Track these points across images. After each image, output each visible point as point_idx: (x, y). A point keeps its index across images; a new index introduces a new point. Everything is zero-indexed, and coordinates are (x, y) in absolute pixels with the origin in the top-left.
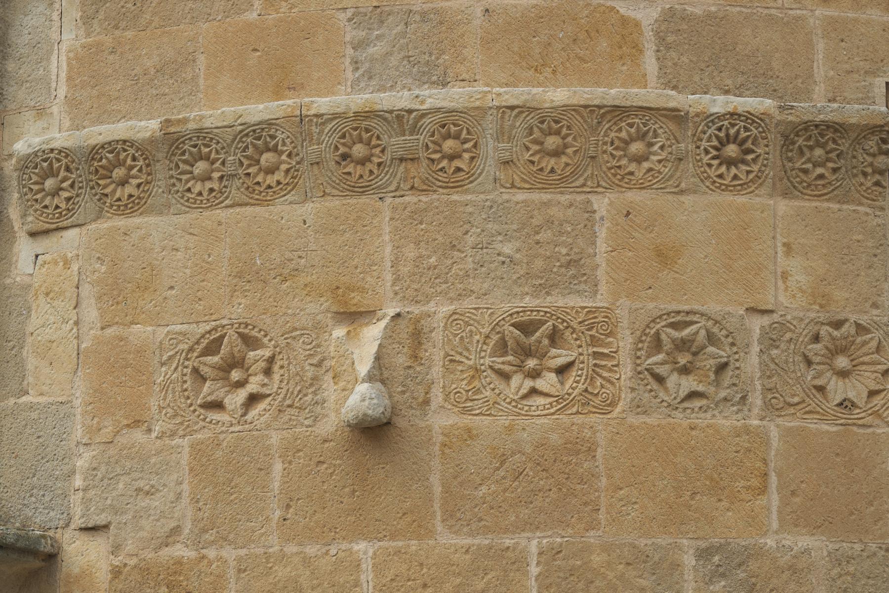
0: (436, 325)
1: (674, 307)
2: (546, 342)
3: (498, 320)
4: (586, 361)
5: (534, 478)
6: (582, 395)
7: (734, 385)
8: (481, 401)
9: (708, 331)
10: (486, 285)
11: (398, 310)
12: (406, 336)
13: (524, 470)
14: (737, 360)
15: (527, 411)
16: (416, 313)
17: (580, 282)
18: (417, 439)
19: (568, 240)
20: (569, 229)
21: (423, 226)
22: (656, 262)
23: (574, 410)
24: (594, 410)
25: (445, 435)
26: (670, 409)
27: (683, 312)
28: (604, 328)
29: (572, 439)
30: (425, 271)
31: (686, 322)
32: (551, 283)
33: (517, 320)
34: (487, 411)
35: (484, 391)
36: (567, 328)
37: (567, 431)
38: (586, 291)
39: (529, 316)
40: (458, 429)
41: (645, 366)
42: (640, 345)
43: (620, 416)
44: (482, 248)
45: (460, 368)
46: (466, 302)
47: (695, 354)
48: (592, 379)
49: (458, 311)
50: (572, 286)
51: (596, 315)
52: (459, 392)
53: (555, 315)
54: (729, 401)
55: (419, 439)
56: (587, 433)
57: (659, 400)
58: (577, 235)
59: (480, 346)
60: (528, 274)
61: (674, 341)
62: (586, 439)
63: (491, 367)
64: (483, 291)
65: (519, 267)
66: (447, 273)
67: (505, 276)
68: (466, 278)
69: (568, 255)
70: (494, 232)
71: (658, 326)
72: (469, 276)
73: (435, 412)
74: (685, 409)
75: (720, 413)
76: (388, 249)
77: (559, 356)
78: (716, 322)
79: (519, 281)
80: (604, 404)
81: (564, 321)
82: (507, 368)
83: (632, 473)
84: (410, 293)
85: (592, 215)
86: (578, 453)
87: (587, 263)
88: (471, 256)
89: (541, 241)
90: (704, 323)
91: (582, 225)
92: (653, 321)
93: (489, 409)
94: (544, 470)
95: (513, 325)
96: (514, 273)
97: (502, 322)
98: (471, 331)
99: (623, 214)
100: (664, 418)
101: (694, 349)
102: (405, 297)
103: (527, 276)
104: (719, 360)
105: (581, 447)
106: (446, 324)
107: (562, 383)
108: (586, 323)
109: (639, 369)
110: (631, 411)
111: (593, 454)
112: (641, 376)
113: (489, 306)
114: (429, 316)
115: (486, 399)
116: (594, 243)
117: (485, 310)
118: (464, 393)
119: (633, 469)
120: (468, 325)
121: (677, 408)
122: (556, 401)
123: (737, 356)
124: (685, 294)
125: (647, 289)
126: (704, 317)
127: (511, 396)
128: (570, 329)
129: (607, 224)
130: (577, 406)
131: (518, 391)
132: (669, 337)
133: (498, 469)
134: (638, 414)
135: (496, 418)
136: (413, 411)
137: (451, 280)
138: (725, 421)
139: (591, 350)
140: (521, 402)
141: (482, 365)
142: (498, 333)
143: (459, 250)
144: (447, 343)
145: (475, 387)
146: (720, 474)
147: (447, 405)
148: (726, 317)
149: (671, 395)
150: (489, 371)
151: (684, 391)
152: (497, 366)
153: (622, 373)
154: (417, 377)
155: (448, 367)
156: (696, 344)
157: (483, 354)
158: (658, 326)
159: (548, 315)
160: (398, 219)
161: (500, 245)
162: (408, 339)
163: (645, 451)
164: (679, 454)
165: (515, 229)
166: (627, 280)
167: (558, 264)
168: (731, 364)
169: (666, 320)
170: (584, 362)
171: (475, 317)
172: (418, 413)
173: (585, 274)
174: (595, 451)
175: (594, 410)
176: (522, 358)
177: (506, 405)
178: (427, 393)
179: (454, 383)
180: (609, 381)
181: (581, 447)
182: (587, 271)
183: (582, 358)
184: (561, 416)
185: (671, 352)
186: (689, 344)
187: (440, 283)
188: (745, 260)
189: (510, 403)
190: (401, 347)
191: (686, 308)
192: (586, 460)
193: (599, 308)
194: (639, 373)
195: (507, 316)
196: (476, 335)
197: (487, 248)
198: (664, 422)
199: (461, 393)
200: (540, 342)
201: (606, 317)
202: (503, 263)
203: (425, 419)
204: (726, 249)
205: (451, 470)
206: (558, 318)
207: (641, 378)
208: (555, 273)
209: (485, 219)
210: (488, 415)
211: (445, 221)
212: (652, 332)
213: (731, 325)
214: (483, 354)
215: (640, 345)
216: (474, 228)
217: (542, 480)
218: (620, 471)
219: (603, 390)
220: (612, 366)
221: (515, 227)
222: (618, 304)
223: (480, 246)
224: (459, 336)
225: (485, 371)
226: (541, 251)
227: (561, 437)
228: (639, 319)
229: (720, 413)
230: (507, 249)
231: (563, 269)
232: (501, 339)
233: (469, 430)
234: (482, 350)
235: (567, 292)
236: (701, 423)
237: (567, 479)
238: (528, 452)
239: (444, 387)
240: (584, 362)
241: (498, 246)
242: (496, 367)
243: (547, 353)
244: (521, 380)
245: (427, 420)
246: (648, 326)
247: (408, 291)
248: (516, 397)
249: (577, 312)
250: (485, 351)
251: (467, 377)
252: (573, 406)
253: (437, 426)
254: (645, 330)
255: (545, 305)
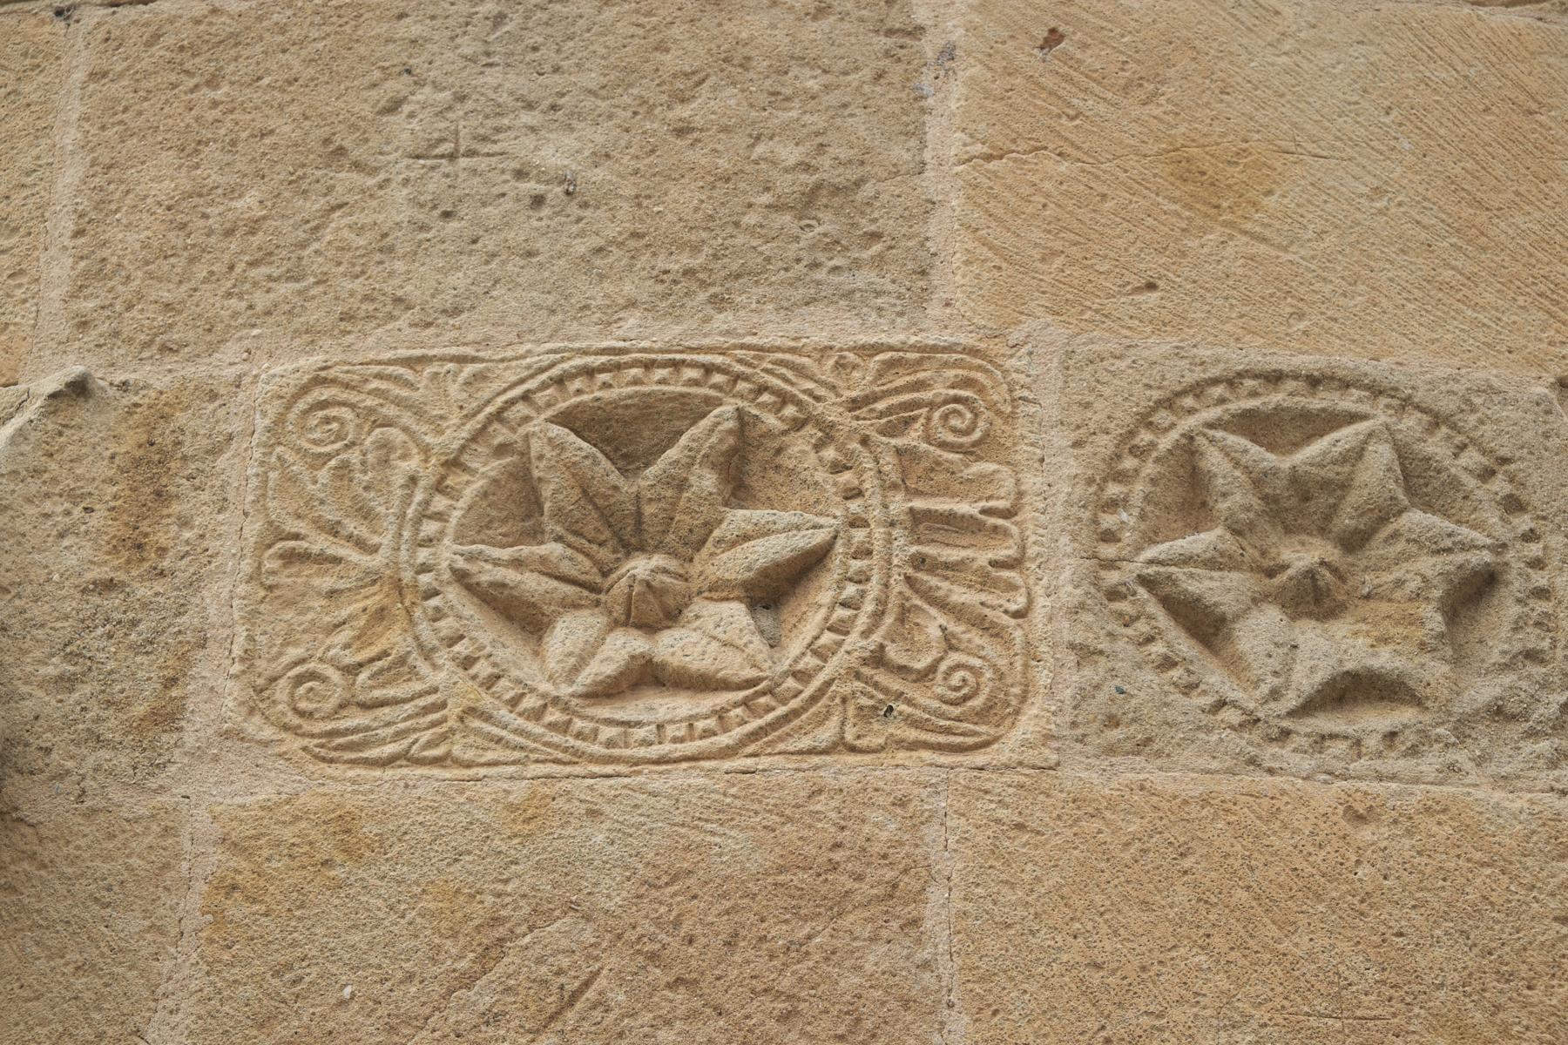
0: (236, 426)
1: (1256, 355)
2: (706, 481)
3: (500, 401)
4: (877, 546)
5: (633, 1015)
6: (858, 676)
7: (1532, 655)
8: (409, 708)
9: (1402, 452)
10: (458, 280)
11: (75, 370)
12: (103, 469)
13: (587, 984)
14: (1537, 564)
15: (610, 743)
16: (158, 386)
17: (857, 264)
18: (105, 868)
19: (807, 118)
20: (811, 84)
21: (219, 94)
22: (1174, 200)
23: (826, 734)
24: (913, 734)
25: (235, 847)
26: (1256, 735)
27: (1296, 377)
28: (955, 422)
29: (810, 850)
30: (213, 240)
31: (1306, 416)
32: (735, 267)
33: (585, 397)
34: (430, 744)
35: (424, 668)
36: (798, 425)
37: (790, 820)
38: (878, 294)
39: (636, 382)
40: (297, 819)
41: (1137, 566)
42: (1113, 489)
43: (1030, 756)
44: (452, 157)
45: (327, 582)
46: (370, 340)
47: (1353, 542)
48: (904, 615)
49: (332, 373)
50: (820, 275)
51: (921, 375)
52: (313, 676)
53: (747, 379)
54: (1513, 717)
55: (118, 866)
56: (879, 826)
57: (1207, 701)
58: (845, 106)
59: (419, 496)
60: (636, 235)
61: (1258, 480)
62: (876, 848)
63: (461, 577)
64: (447, 299)
65: (601, 213)
66: (303, 245)
67: (541, 244)
68: (378, 257)
69: (807, 167)
70: (504, 98)
71: (1191, 422)
72: (390, 249)
73: (197, 754)
74: (1323, 739)
75: (1479, 761)
76: (70, 176)
77: (764, 532)
78: (1437, 420)
79: (598, 262)
80: (956, 711)
81: (784, 399)
82: (532, 584)
83: (1086, 991)
84: (146, 316)
85: (908, 41)
86: (838, 905)
87: (885, 197)
88: (406, 182)
89: (698, 122)
90: (1383, 418)
91: (867, 73)
92: (1168, 403)
93: (444, 737)
94: (679, 981)
95: (566, 419)
96: (582, 234)
97: (521, 409)
98: (385, 446)
99: (1035, 39)
100: (1231, 772)
101: (1346, 520)
102: (116, 334)
103: (632, 243)
104: (1459, 558)
105: (850, 884)
106: (280, 420)
107: (774, 643)
108: (881, 406)
109: (1112, 577)
110: (1081, 740)
111: (910, 911)
112: (1124, 606)
113: (469, 351)
114: (213, 396)
115: (430, 699)
116: (915, 133)
117: (450, 366)
118: (335, 676)
119: (1096, 977)
120: (375, 425)
121: (1286, 734)
122: (745, 703)
123: (1535, 549)
124: (1301, 316)
125: (1138, 290)
126: (1383, 401)
127: (545, 687)
128: (809, 430)
129: (969, 69)
130: (835, 720)
131: (576, 670)
132: (1237, 464)
133: (467, 980)
134: (1111, 750)
135: (472, 772)
136: (104, 754)
137: (318, 265)
138: (1498, 795)
139: (899, 504)
140: (591, 711)
141: (424, 568)
142: (502, 450)
143: (357, 166)
144: (279, 489)
145: (385, 654)
146: (1498, 1008)
147: (255, 727)
148: (1478, 401)
149: (1256, 684)
150: (453, 594)
151: (1313, 670)
152: (487, 574)
153: (1039, 590)
154: (134, 623)
155: (271, 581)
156: (1354, 498)
157: (430, 527)
158: (1191, 422)
159: (718, 378)
160: (121, 75)
161: (530, 141)
162: (112, 481)
163: (1145, 905)
164: (1303, 920)
165: (593, 86)
166: (1055, 253)
167: (766, 198)
168: (1512, 575)
169: (1222, 401)
170: (869, 553)
171: (405, 393)
172: (123, 760)
173: (876, 236)
174: (919, 897)
175: (913, 734)
176: (604, 554)
177: (520, 721)
178: (171, 682)
179: (296, 644)
180: (981, 623)
181: (850, 884)
182: (888, 225)
183: (859, 535)
184: (764, 762)
185: (1251, 526)
186: (1323, 501)
187: (270, 278)
188: (1537, 215)
189: (536, 715)
190: (77, 512)
191: (1309, 362)
192: (873, 939)
193: (935, 349)
194: (1114, 594)
195: (544, 386)
196: (404, 457)
197: (471, 153)
198: (1227, 787)
199: (324, 679)
200: (682, 485)
201: (968, 383)
202: (538, 201)
203: (153, 783)
204: (1458, 170)
205: (250, 991)
206: (763, 389)
207: (1121, 615)
208: (751, 230)
209: (472, 60)
210: (437, 761)
211: (311, 71)
212: (1165, 443)
213: (1500, 433)
214: (430, 527)
215: (1113, 489)
216: (427, 89)
217: (668, 1023)
218: (1032, 987)
219: (955, 658)
220: (994, 564)
221: (592, 79)
222: (1016, 336)
223: (446, 148)
224: (333, 463)
225: (436, 593)
226: (698, 156)
227: (760, 844)
228: (1107, 391)
229: (1479, 761)
230: (555, 153)
231: (786, 218)
232: (513, 476)
233: (344, 824)
234: (424, 515)
235: (800, 293)
236: (1399, 795)
237: (785, 1017)
238: (610, 905)
239: (248, 657)
240: (869, 553)
241: (521, 147)
242: (484, 578)
243: (709, 526)
244: (594, 632)
245: (161, 789)
246: (1145, 421)
247: (134, 312)
248: (565, 691)
249: (840, 365)
250: (440, 516)
251: (352, 617)
252: (822, 720)
253: (202, 814)
254: (1132, 433)
255: (706, 342)
